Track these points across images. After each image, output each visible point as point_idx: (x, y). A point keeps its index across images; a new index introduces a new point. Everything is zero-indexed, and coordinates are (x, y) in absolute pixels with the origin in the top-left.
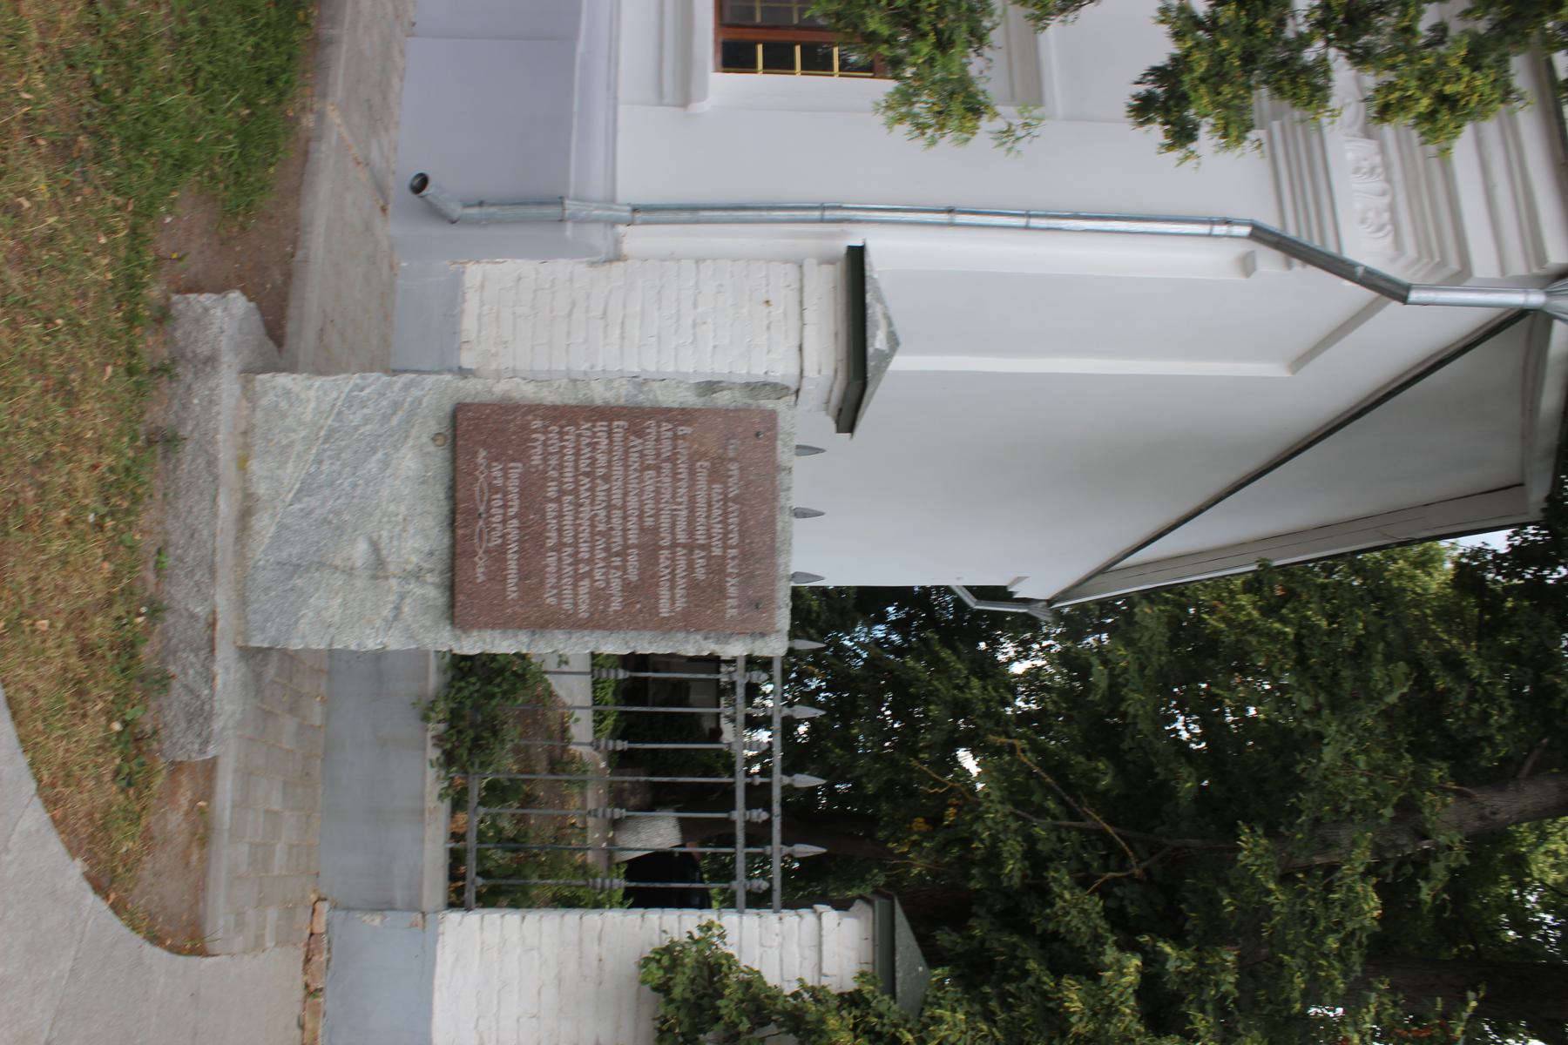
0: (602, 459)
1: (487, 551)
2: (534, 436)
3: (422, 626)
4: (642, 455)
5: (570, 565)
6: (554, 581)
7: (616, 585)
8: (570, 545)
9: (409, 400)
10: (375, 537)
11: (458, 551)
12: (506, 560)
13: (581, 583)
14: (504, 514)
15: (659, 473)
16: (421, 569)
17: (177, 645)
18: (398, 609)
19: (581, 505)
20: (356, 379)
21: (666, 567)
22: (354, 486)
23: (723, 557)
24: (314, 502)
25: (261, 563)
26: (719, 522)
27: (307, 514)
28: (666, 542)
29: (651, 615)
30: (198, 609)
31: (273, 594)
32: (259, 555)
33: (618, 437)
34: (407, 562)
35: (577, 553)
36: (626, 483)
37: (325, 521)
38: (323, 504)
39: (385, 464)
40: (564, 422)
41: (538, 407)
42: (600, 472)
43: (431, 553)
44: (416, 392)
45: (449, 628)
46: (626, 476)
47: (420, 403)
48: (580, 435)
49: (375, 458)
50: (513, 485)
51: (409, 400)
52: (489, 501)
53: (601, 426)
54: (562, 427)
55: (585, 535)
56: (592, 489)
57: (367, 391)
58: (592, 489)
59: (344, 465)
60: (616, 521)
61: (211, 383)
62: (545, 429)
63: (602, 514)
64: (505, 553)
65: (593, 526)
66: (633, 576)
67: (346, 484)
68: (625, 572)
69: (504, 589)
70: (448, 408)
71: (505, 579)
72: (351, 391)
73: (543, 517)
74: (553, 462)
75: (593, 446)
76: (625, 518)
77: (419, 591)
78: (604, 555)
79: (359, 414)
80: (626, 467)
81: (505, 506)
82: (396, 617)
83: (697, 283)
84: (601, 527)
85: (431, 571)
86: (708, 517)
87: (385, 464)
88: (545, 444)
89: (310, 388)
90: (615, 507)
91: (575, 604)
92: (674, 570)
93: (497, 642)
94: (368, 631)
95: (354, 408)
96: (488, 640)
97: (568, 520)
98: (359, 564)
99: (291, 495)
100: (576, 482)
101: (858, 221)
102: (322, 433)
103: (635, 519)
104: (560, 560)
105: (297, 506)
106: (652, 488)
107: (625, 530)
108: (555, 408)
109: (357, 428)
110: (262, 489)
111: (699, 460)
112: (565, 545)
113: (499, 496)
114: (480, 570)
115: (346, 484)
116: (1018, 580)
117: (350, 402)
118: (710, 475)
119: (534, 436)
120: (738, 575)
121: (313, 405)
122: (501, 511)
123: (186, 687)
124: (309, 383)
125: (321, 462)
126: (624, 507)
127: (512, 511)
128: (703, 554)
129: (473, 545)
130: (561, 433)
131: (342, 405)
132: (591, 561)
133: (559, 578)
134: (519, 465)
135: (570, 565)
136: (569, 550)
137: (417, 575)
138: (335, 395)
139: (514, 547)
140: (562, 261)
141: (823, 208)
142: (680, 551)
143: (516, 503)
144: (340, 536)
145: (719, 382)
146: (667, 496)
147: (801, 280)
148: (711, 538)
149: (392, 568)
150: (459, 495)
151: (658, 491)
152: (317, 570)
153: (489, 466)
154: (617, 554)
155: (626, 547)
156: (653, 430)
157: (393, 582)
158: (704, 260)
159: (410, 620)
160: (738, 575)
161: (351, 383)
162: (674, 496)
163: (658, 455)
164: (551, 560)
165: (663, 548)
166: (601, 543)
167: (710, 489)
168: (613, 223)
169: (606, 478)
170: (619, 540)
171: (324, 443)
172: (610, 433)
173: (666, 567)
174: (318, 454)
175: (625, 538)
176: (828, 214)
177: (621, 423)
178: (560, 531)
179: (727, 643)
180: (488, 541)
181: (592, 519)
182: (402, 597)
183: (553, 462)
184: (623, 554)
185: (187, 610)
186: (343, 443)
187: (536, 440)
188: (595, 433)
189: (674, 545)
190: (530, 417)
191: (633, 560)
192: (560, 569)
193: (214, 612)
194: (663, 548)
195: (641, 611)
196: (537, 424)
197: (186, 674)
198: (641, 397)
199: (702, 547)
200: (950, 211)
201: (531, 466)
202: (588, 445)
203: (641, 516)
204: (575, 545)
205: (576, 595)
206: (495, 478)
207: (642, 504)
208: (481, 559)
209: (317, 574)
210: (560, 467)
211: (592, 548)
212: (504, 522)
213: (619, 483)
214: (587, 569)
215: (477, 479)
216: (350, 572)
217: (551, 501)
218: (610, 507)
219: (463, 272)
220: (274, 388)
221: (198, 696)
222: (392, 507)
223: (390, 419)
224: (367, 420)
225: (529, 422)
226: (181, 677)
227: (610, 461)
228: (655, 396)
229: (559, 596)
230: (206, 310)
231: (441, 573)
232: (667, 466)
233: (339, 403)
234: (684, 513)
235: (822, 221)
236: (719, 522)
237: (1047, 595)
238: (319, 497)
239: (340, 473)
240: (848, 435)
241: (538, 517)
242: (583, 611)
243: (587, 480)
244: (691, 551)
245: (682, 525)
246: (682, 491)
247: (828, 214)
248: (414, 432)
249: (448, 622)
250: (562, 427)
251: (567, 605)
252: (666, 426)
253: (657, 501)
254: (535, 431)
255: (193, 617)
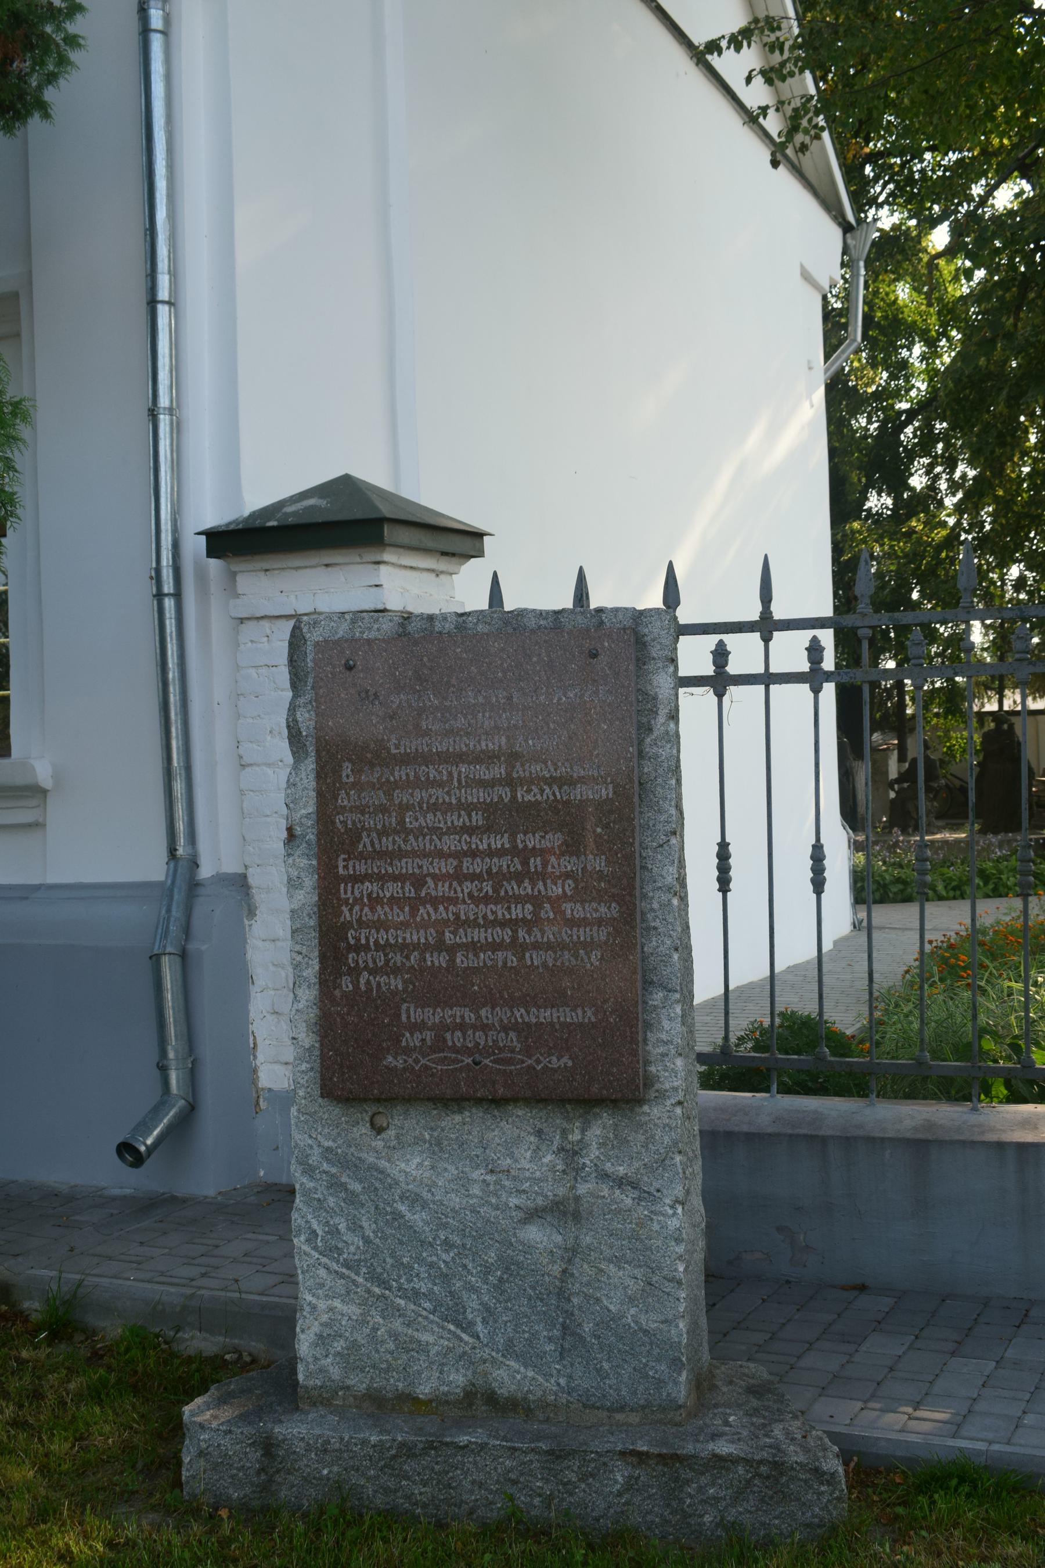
0: (392, 889)
1: (528, 1052)
2: (363, 988)
4: (384, 832)
6: (567, 955)
7: (569, 864)
9: (325, 1166)
10: (519, 1215)
12: (539, 1025)
14: (475, 1028)
15: (409, 807)
16: (561, 1149)
17: (674, 1512)
18: (621, 1182)
19: (457, 916)
20: (299, 1242)
21: (542, 791)
22: (448, 1245)
24: (472, 1303)
25: (562, 1381)
27: (488, 1312)
28: (505, 793)
29: (611, 812)
30: (620, 1479)
31: (606, 1365)
32: (551, 1385)
33: (361, 868)
34: (552, 1169)
35: (524, 920)
37: (499, 1287)
38: (473, 1289)
39: (415, 1200)
42: (409, 891)
43: (539, 1133)
44: (315, 1158)
45: (646, 1108)
47: (328, 1149)
48: (359, 921)
49: (409, 1216)
50: (433, 1016)
52: (454, 1049)
53: (346, 892)
55: (500, 911)
56: (435, 902)
57: (315, 1226)
58: (435, 902)
59: (420, 1260)
60: (478, 866)
61: (299, 1447)
62: (355, 972)
63: (468, 886)
65: (486, 899)
66: (554, 840)
67: (444, 1256)
68: (549, 851)
69: (581, 1025)
70: (335, 1111)
71: (565, 1025)
72: (315, 1248)
73: (476, 970)
75: (375, 901)
76: (474, 854)
77: (594, 1152)
79: (348, 1237)
80: (401, 854)
81: (462, 1027)
82: (635, 1185)
83: (269, 765)
84: (488, 887)
85: (564, 1133)
87: (415, 1200)
88: (374, 971)
89: (314, 1308)
91: (600, 922)
94: (656, 1227)
95: (340, 1245)
97: (478, 935)
98: (559, 1239)
99: (464, 1336)
100: (424, 925)
101: (176, 545)
102: (377, 1290)
104: (536, 946)
105: (479, 1327)
107: (491, 853)
108: (323, 958)
109: (367, 1241)
110: (458, 1379)
112: (514, 938)
113: (448, 1036)
114: (555, 1062)
115: (444, 1256)
116: (806, 276)
117: (331, 1251)
119: (363, 988)
121: (337, 1303)
122: (470, 1032)
123: (736, 1500)
124: (307, 1309)
125: (416, 1293)
126: (459, 855)
127: (470, 1016)
130: (358, 948)
131: (338, 1262)
132: (537, 901)
134: (404, 1006)
136: (521, 933)
137: (571, 1154)
138: (322, 1272)
139: (520, 1013)
140: (250, 954)
141: (159, 596)
142: (519, 772)
143: (457, 1011)
144: (517, 1264)
146: (439, 794)
147: (258, 619)
148: (497, 727)
149: (561, 1191)
151: (434, 808)
152: (569, 1300)
153: (408, 1051)
154: (525, 863)
155: (514, 851)
157: (582, 1189)
158: (241, 757)
159: (636, 1164)
161: (306, 1248)
162: (441, 785)
163: (383, 810)
164: (536, 958)
165: (514, 797)
166: (512, 888)
168: (194, 886)
169: (419, 882)
171: (390, 1289)
172: (357, 879)
174: (404, 1297)
175: (501, 853)
176: (168, 587)
178: (495, 947)
179: (655, 698)
180: (512, 1051)
181: (476, 900)
182: (604, 1176)
184: (525, 855)
185: (620, 1494)
186: (389, 1260)
187: (368, 982)
188: (356, 900)
189: (510, 782)
190: (337, 993)
191: (532, 841)
192: (549, 947)
193: (623, 1454)
194: (514, 797)
196: (346, 984)
197: (717, 1499)
198: (311, 837)
200: (153, 414)
201: (405, 990)
202: (373, 909)
203: (471, 830)
204: (513, 924)
205: (583, 922)
206: (423, 1040)
207: (453, 830)
209: (575, 1300)
210: (405, 948)
211: (520, 900)
213: (425, 862)
214: (547, 906)
215: (426, 1068)
216: (572, 1253)
217: (452, 960)
218: (459, 876)
219: (270, 1090)
220: (316, 1359)
221: (749, 1482)
222: (476, 1190)
223: (353, 1193)
224: (355, 1227)
225: (345, 995)
226: (722, 1505)
228: (308, 816)
229: (588, 946)
230: (201, 1454)
231: (569, 1120)
232: (401, 796)
233: (334, 1266)
235: (178, 595)
237: (834, 234)
238: (465, 1295)
239: (431, 1265)
241: (476, 980)
242: (612, 911)
243: (422, 910)
245: (482, 772)
247: (168, 587)
248: (371, 1159)
250: (350, 948)
251: (602, 934)
252: (343, 801)
253: (448, 808)
255: (630, 1485)
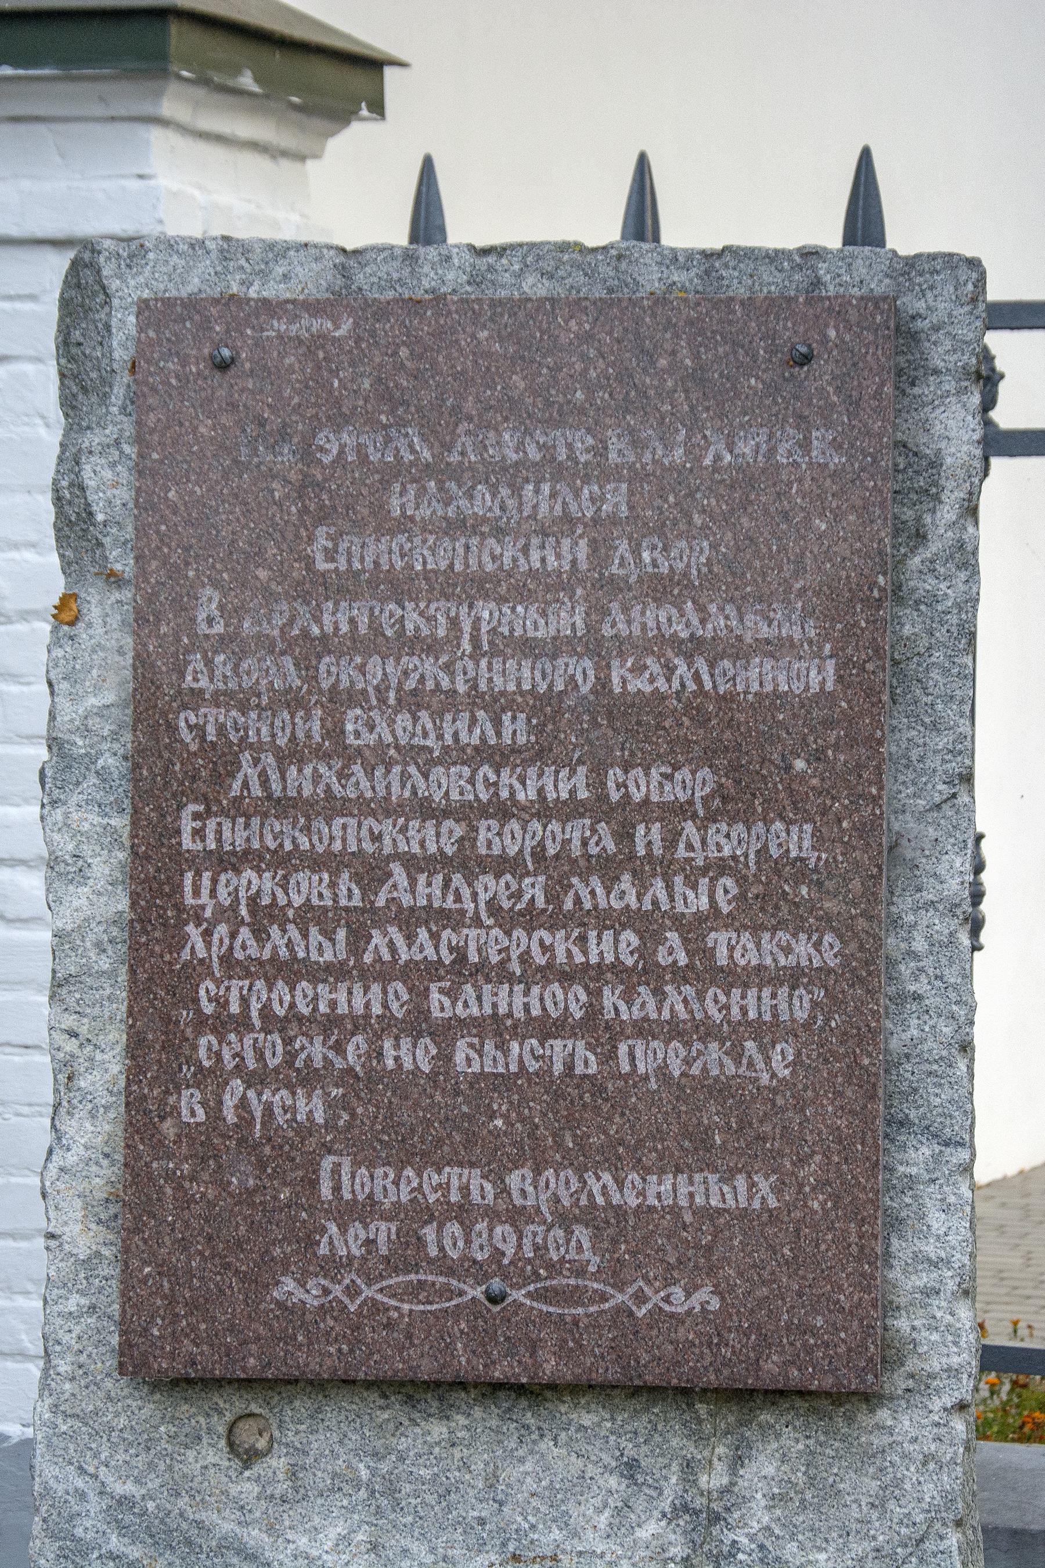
2: (231, 1117)
3: (878, 1505)
5: (659, 993)
8: (596, 994)
11: (613, 1374)
12: (644, 1211)
13: (722, 958)
14: (493, 1215)
15: (354, 698)
21: (670, 670)
23: (636, 477)
26: (517, 491)
35: (617, 967)
36: (386, 809)
40: (185, 1015)
41: (134, 1103)
43: (630, 1469)
45: (883, 1415)
46: (364, 807)
48: (227, 960)
51: (115, 1542)
54: (201, 1023)
55: (562, 945)
63: (488, 885)
64: (620, 1212)
68: (683, 810)
73: (503, 1082)
74: (317, 1050)
78: (626, 882)
84: (535, 889)
85: (689, 1468)
86: (499, 533)
88: (256, 1080)
90: (467, 841)
91: (795, 977)
92: (675, 641)
93: (930, 1249)
96: (923, 1279)
103: (506, 776)
104: (644, 1029)
106: (404, 720)
111: (309, 563)
112: (593, 1011)
113: (429, 1233)
114: (679, 1301)
118: (359, 526)
119: (231, 1117)
120: (694, 426)
122: (481, 1226)
128: (623, 547)
129: (595, 1323)
133: (706, 1031)
134: (328, 1162)
135: (659, 993)
143: (453, 1175)
145: (58, 500)
150: (427, 1370)
153: (332, 1267)
154: (625, 836)
156: (212, 717)
160: (694, 426)
162: (431, 647)
163: (294, 702)
165: (603, 685)
167: (404, 525)
170: (576, 831)
173: (670, 670)
177: (187, 825)
183: (317, 1050)
187: (243, 1104)
190: (168, 1128)
192: (674, 1031)
194: (603, 685)
195: (817, 756)
199: (600, 550)
202: (260, 934)
208: (640, 1298)
212: (517, 1217)
213: (387, 827)
217: (445, 1057)
225: (186, 1132)
227: (316, 863)
228: (101, 712)
234: (485, 611)
236: (517, 491)
240: (389, 72)
244: (614, 586)
246: (413, 620)
248: (226, 1525)
249: (864, 1419)
250: (201, 1023)
254: (215, 1112)
